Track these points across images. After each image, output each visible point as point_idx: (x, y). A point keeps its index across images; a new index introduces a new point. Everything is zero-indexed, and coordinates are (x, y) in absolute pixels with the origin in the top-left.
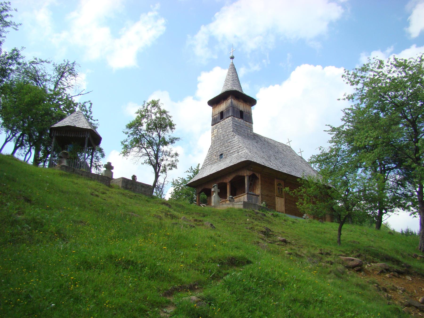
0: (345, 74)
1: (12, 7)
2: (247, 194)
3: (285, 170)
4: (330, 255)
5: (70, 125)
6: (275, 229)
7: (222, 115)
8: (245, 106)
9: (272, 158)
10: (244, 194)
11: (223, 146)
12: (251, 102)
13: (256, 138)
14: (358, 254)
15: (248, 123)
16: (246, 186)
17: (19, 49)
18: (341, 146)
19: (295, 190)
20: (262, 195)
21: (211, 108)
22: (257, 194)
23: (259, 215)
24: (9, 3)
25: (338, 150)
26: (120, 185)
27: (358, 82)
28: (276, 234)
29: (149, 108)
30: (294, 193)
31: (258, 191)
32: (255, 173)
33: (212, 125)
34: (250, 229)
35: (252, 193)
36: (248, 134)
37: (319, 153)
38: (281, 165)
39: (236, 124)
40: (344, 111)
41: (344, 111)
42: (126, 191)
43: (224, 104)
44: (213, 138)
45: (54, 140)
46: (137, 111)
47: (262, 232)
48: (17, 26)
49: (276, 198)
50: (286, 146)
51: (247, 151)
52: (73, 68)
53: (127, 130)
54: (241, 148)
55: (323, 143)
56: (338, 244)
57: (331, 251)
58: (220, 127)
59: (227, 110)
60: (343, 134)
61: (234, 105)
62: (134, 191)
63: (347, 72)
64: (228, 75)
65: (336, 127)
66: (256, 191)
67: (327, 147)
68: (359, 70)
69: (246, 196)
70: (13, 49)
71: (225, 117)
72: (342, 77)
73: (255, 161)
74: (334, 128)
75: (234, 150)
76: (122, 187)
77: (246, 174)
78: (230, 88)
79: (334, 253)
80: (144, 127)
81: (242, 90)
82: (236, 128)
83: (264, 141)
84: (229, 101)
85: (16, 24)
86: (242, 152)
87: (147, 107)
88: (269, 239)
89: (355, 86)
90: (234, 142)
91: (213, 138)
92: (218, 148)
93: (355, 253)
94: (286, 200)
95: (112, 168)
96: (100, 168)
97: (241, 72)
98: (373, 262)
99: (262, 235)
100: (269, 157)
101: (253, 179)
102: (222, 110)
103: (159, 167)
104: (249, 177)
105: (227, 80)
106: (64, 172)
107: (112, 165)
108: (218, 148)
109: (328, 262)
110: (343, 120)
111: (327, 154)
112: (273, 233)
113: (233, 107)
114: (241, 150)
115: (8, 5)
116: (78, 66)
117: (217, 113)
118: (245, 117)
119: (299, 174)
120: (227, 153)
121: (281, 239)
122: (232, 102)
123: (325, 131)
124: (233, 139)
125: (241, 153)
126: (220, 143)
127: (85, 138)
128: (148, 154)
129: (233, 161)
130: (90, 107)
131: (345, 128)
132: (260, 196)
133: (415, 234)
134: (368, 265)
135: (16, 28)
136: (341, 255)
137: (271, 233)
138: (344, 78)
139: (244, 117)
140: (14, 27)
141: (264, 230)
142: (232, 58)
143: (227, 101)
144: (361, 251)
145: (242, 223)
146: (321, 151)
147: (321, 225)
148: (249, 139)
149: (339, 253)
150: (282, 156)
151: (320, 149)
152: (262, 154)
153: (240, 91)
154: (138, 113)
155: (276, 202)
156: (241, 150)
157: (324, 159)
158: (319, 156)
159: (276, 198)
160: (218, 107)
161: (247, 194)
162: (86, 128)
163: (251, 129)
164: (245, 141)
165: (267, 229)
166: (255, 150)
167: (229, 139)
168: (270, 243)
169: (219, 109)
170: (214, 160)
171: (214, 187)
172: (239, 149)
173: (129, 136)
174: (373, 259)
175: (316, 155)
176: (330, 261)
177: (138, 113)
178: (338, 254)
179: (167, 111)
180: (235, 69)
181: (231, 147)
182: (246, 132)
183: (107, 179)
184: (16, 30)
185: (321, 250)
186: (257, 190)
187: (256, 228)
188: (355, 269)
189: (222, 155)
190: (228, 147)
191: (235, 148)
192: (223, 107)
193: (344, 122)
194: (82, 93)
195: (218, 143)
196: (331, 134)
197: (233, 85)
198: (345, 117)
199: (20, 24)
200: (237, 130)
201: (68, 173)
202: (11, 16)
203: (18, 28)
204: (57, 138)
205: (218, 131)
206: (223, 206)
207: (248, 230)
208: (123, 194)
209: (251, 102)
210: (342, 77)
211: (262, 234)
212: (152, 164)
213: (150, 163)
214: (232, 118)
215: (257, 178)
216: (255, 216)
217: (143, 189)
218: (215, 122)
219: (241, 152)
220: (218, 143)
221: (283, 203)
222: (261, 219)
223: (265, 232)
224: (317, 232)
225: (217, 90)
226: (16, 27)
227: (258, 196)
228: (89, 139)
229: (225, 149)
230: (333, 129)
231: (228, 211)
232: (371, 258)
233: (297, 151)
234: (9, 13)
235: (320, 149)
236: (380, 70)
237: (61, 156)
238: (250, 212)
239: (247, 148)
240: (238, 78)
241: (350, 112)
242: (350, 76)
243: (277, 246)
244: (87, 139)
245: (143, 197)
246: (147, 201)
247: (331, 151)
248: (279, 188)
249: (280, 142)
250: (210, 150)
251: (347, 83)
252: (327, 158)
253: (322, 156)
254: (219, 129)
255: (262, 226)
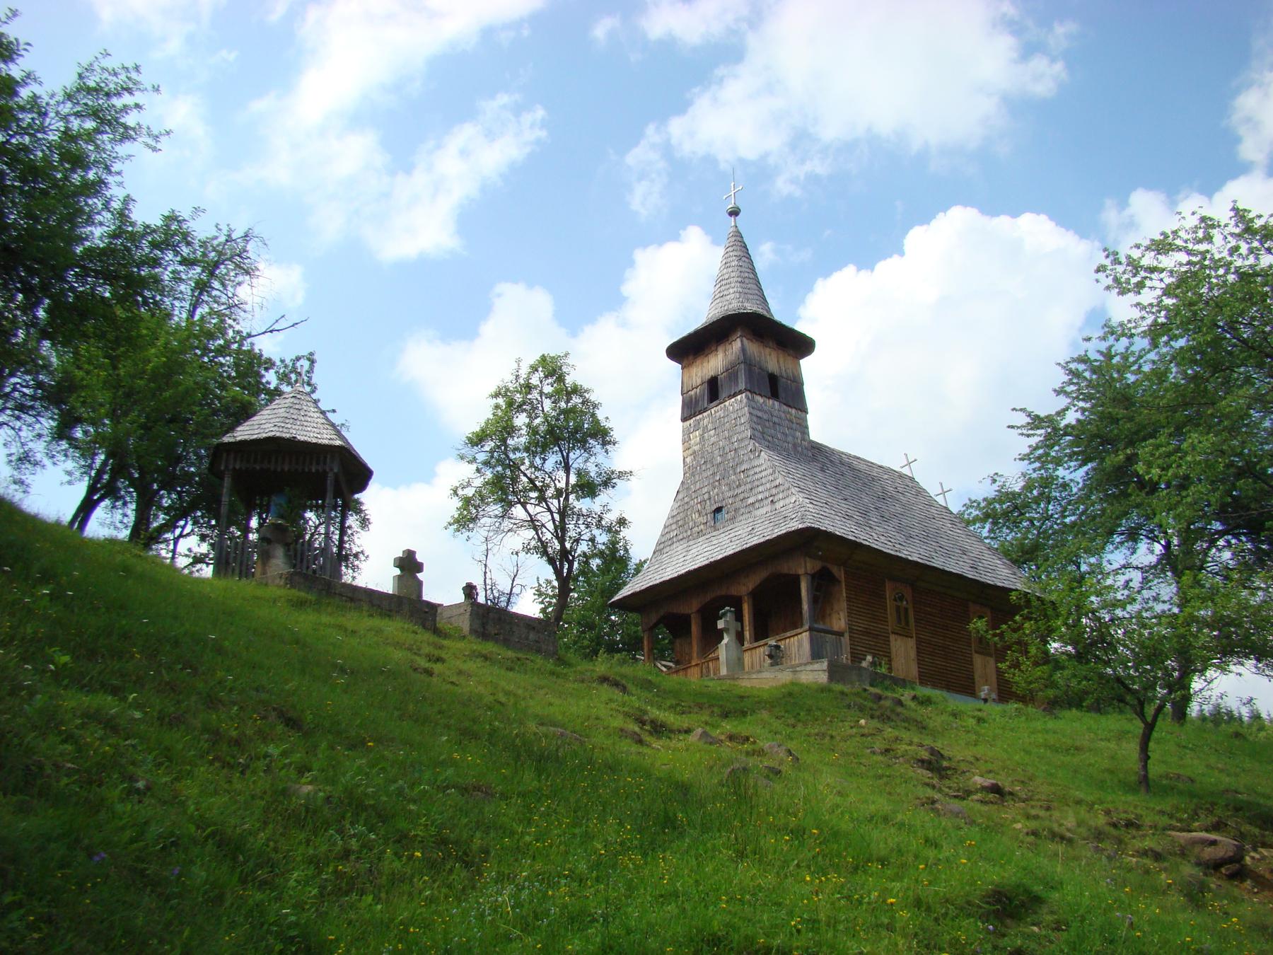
0: (1107, 262)
1: (145, 79)
2: (811, 629)
3: (913, 553)
4: (1138, 827)
5: (278, 434)
6: (955, 749)
7: (714, 390)
8: (781, 360)
9: (874, 517)
10: (799, 630)
11: (723, 482)
12: (800, 345)
13: (819, 456)
14: (1212, 819)
15: (793, 411)
16: (805, 607)
17: (185, 213)
18: (1055, 470)
19: (1004, 626)
20: (851, 631)
21: (675, 367)
22: (836, 628)
23: (888, 703)
24: (137, 68)
25: (1046, 482)
26: (465, 624)
27: (1140, 285)
28: (963, 766)
29: (535, 380)
30: (1001, 635)
31: (839, 622)
32: (829, 566)
33: (684, 419)
34: (882, 753)
35: (821, 626)
36: (795, 446)
37: (990, 491)
38: (901, 539)
39: (760, 414)
40: (1065, 367)
41: (1065, 367)
42: (489, 647)
43: (720, 355)
44: (688, 460)
45: (227, 482)
46: (493, 390)
47: (922, 761)
48: (156, 138)
49: (892, 637)
50: (901, 476)
51: (800, 497)
52: (245, 251)
53: (469, 451)
54: (781, 488)
55: (1005, 463)
56: (1143, 789)
57: (1139, 817)
58: (710, 426)
59: (731, 372)
60: (1066, 434)
61: (746, 356)
62: (507, 643)
63: (1111, 258)
64: (726, 265)
65: (1042, 415)
66: (834, 621)
67: (1014, 475)
68: (1148, 248)
69: (805, 636)
70: (167, 214)
71: (723, 395)
72: (1098, 271)
73: (831, 529)
74: (1037, 416)
75: (760, 497)
76: (473, 631)
77: (804, 568)
78: (734, 303)
79: (1148, 821)
80: (520, 440)
81: (768, 311)
82: (759, 428)
83: (841, 463)
84: (736, 346)
85: (155, 132)
86: (787, 501)
87: (528, 379)
88: (947, 782)
89: (1131, 298)
90: (757, 470)
91: (688, 460)
92: (705, 490)
93: (1203, 816)
94: (919, 643)
95: (419, 567)
96: (356, 563)
97: (764, 256)
98: (1264, 845)
99: (925, 774)
100: (865, 514)
101: (823, 582)
102: (712, 373)
103: (571, 564)
104: (813, 576)
105: (721, 282)
106: (303, 594)
107: (419, 558)
108: (705, 490)
109: (1144, 853)
110: (1059, 392)
111: (1014, 495)
112: (954, 765)
113: (747, 361)
114: (781, 496)
115: (134, 75)
116: (260, 244)
117: (699, 382)
118: (784, 392)
119: (953, 562)
120: (738, 504)
121: (986, 784)
122: (743, 349)
123: (1012, 427)
124: (756, 463)
125: (781, 503)
126: (714, 474)
127: (325, 473)
128: (533, 523)
129: (759, 529)
130: (311, 371)
131: (1072, 417)
132: (847, 635)
133: (1240, 718)
134: (1252, 854)
135: (153, 144)
136: (1174, 828)
137: (945, 764)
138: (1101, 276)
139: (782, 394)
140: (150, 141)
141: (925, 755)
142: (734, 213)
143: (729, 347)
144: (1218, 812)
145: (851, 736)
146: (995, 487)
147: (1051, 724)
148: (799, 461)
149: (1165, 820)
150: (899, 509)
151: (994, 481)
152: (843, 504)
153: (765, 313)
154: (496, 395)
155: (893, 650)
156: (781, 496)
157: (1004, 510)
158: (990, 502)
159: (892, 637)
160: (698, 362)
161: (811, 629)
162: (326, 442)
163: (804, 428)
164: (792, 466)
165: (933, 751)
166: (823, 494)
167: (742, 463)
168: (956, 797)
169: (705, 371)
170: (696, 525)
171: (724, 614)
172: (774, 491)
173: (478, 470)
174: (1263, 836)
175: (980, 499)
176: (1152, 850)
177: (496, 395)
178: (1161, 825)
179: (585, 387)
180: (745, 247)
181: (749, 486)
182: (790, 439)
183: (407, 602)
184: (155, 149)
185: (1108, 812)
186: (835, 616)
187: (903, 747)
188: (1223, 870)
189: (719, 510)
190: (739, 486)
191: (760, 489)
192: (715, 363)
193: (1063, 401)
194: (276, 327)
195: (705, 475)
196: (1028, 436)
197: (744, 294)
198: (1070, 383)
199: (168, 133)
200: (763, 433)
201: (311, 597)
202: (137, 106)
203: (159, 146)
204: (238, 477)
205: (702, 436)
206: (760, 676)
207: (880, 758)
208: (486, 658)
209: (800, 345)
210: (1098, 271)
211: (922, 767)
212: (545, 553)
213: (543, 549)
214: (747, 397)
215: (833, 580)
216: (875, 706)
217: (532, 636)
218: (691, 409)
219: (779, 505)
220: (705, 475)
221: (913, 654)
222: (893, 716)
223: (930, 762)
224: (1055, 750)
225: (700, 315)
226: (155, 139)
227: (840, 634)
228: (336, 475)
229: (731, 493)
230: (1037, 422)
231: (790, 694)
232: (1257, 831)
233: (932, 489)
234: (139, 98)
235: (994, 481)
236: (1202, 247)
237: (268, 536)
238: (857, 694)
239: (802, 490)
240: (755, 275)
241: (1081, 367)
242: (1120, 269)
243: (978, 806)
244: (331, 476)
245: (539, 660)
246: (552, 673)
247: (1028, 487)
248: (898, 608)
249: (884, 465)
250: (680, 496)
251: (1108, 288)
252: (1016, 507)
253: (1001, 502)
254: (705, 429)
255: (911, 744)
